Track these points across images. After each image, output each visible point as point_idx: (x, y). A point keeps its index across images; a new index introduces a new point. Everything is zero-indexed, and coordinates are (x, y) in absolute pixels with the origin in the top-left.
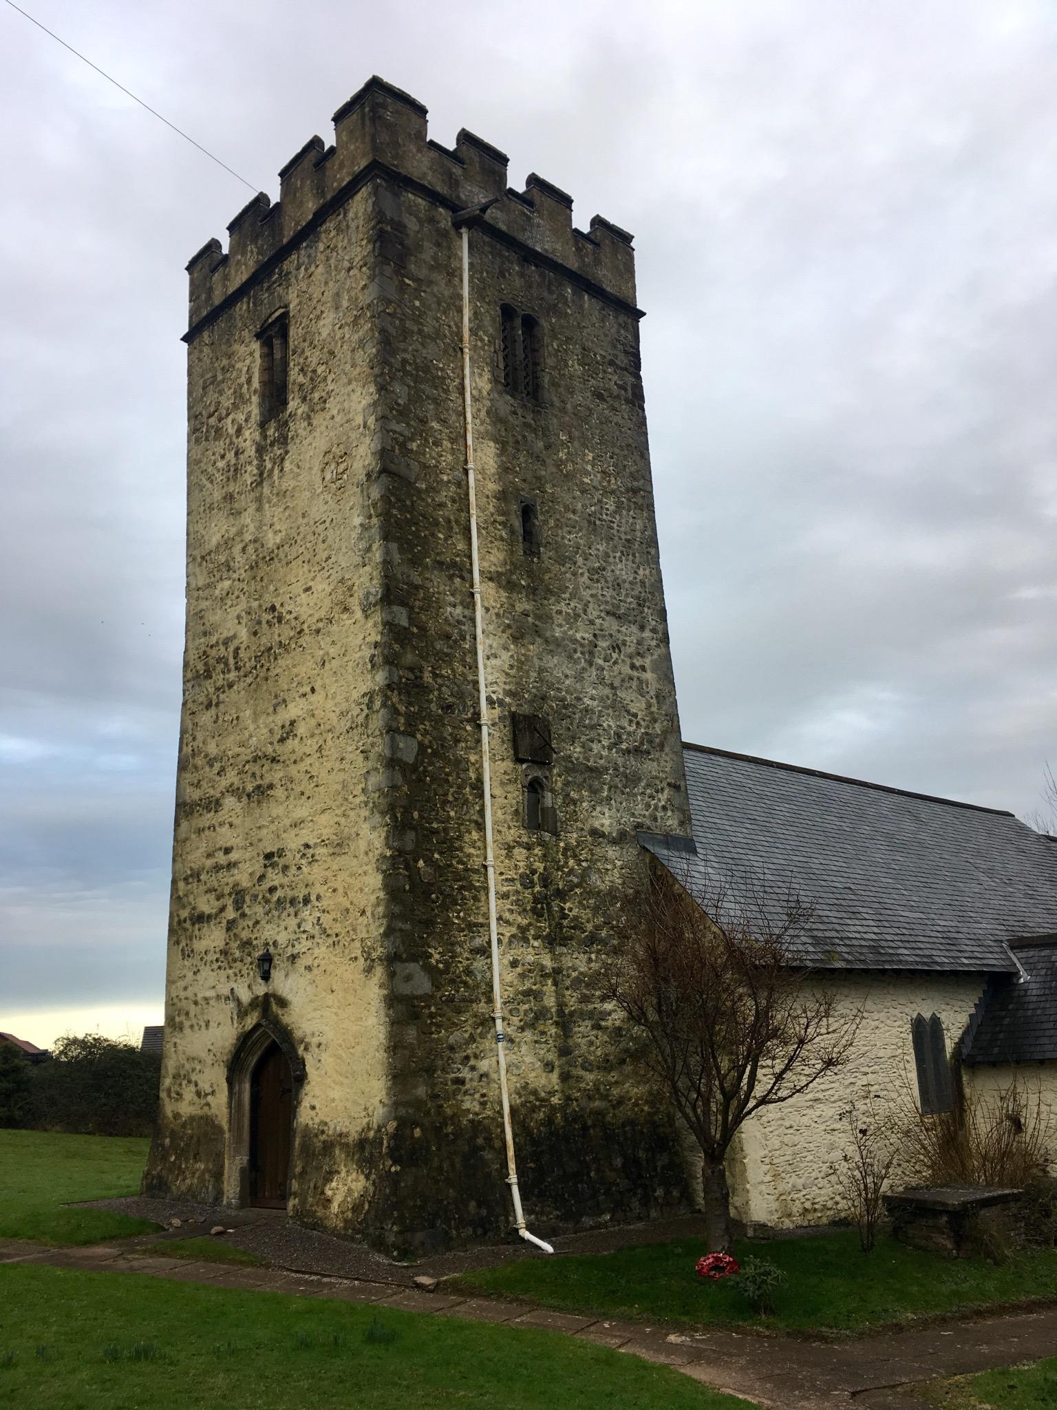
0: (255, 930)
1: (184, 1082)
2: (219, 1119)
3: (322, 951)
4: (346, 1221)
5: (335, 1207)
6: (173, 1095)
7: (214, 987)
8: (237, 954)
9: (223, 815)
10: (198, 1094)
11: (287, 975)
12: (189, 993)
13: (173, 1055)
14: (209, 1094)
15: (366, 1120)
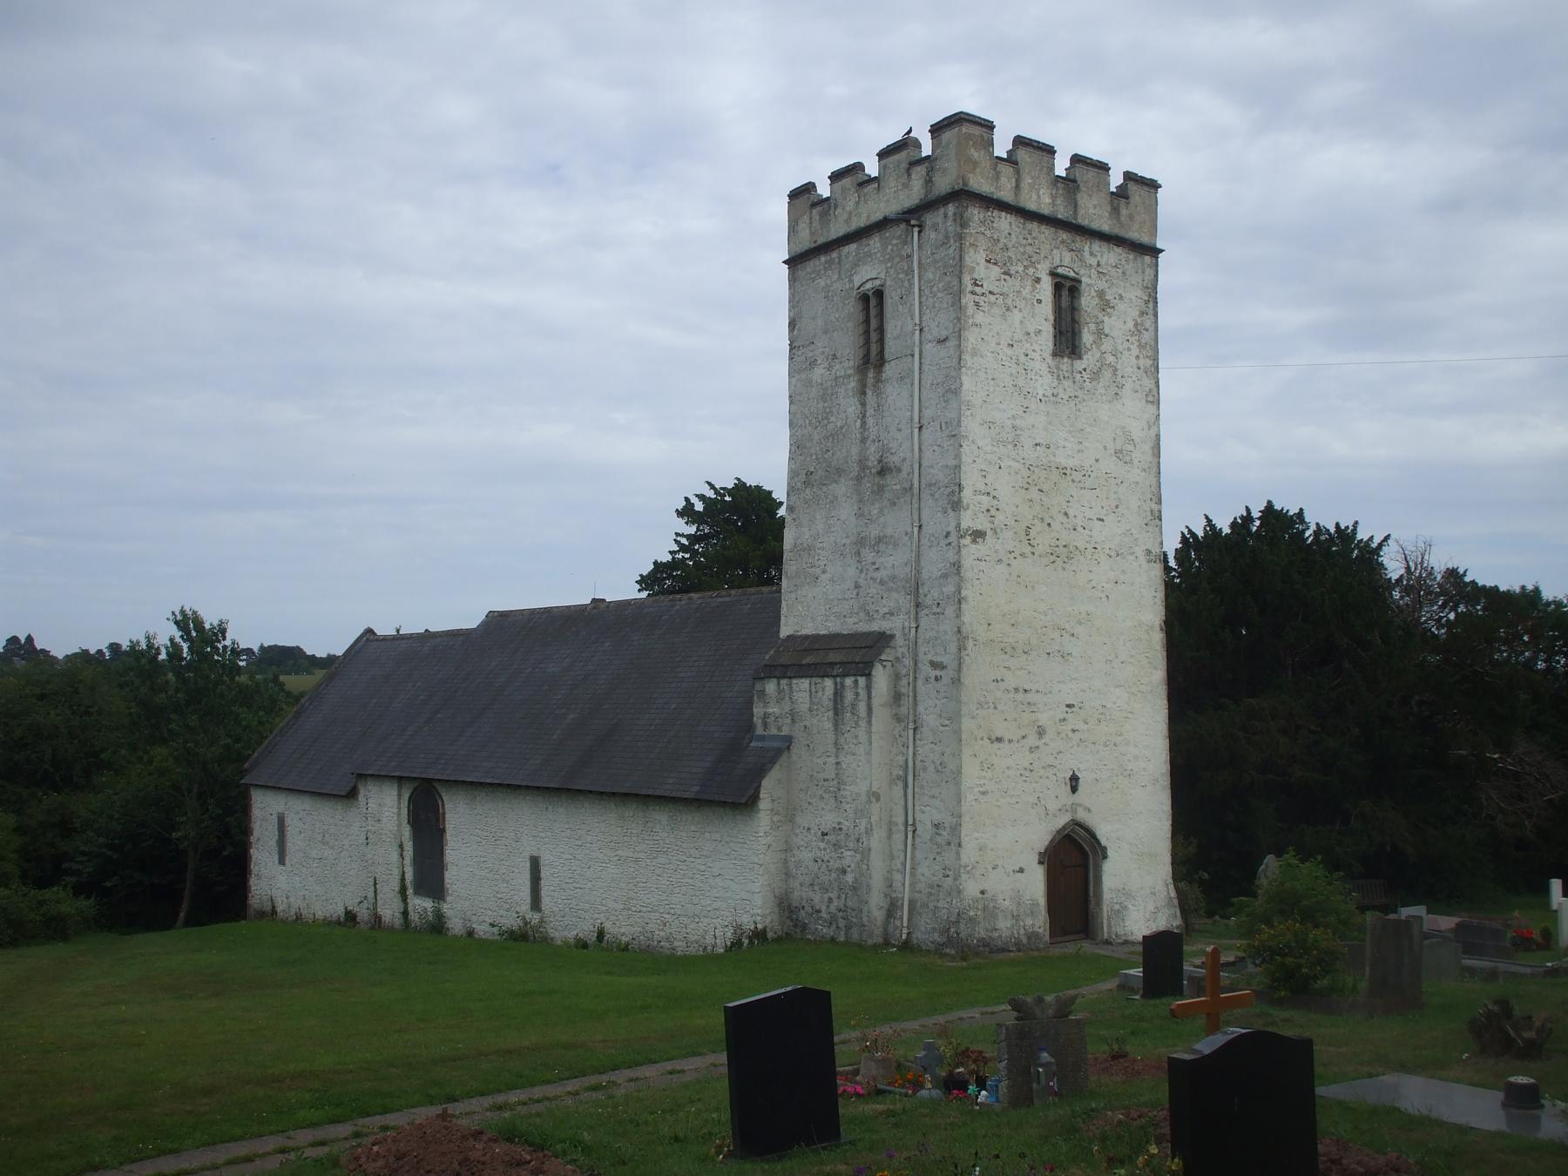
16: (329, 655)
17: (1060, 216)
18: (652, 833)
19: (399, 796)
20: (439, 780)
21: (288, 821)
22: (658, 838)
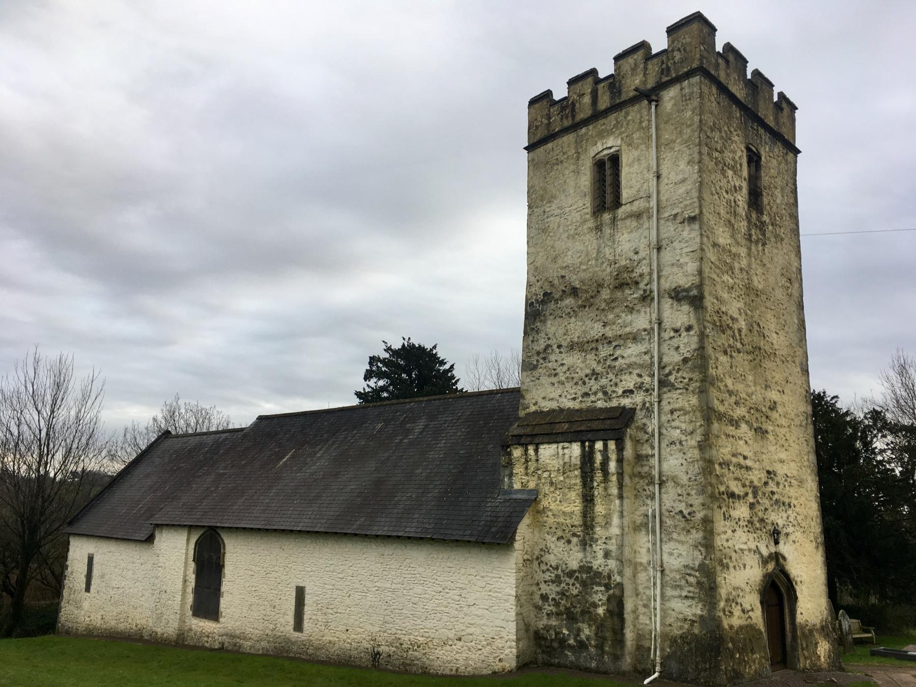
0: (766, 514)
1: (733, 605)
2: (758, 625)
3: (798, 534)
4: (828, 664)
5: (822, 659)
6: (727, 613)
7: (746, 543)
8: (758, 525)
9: (738, 433)
10: (743, 611)
11: (785, 543)
12: (730, 544)
13: (724, 586)
14: (750, 611)
15: (821, 617)
17: (759, 114)
18: (410, 569)
19: (188, 540)
20: (223, 528)
21: (96, 560)
22: (415, 572)
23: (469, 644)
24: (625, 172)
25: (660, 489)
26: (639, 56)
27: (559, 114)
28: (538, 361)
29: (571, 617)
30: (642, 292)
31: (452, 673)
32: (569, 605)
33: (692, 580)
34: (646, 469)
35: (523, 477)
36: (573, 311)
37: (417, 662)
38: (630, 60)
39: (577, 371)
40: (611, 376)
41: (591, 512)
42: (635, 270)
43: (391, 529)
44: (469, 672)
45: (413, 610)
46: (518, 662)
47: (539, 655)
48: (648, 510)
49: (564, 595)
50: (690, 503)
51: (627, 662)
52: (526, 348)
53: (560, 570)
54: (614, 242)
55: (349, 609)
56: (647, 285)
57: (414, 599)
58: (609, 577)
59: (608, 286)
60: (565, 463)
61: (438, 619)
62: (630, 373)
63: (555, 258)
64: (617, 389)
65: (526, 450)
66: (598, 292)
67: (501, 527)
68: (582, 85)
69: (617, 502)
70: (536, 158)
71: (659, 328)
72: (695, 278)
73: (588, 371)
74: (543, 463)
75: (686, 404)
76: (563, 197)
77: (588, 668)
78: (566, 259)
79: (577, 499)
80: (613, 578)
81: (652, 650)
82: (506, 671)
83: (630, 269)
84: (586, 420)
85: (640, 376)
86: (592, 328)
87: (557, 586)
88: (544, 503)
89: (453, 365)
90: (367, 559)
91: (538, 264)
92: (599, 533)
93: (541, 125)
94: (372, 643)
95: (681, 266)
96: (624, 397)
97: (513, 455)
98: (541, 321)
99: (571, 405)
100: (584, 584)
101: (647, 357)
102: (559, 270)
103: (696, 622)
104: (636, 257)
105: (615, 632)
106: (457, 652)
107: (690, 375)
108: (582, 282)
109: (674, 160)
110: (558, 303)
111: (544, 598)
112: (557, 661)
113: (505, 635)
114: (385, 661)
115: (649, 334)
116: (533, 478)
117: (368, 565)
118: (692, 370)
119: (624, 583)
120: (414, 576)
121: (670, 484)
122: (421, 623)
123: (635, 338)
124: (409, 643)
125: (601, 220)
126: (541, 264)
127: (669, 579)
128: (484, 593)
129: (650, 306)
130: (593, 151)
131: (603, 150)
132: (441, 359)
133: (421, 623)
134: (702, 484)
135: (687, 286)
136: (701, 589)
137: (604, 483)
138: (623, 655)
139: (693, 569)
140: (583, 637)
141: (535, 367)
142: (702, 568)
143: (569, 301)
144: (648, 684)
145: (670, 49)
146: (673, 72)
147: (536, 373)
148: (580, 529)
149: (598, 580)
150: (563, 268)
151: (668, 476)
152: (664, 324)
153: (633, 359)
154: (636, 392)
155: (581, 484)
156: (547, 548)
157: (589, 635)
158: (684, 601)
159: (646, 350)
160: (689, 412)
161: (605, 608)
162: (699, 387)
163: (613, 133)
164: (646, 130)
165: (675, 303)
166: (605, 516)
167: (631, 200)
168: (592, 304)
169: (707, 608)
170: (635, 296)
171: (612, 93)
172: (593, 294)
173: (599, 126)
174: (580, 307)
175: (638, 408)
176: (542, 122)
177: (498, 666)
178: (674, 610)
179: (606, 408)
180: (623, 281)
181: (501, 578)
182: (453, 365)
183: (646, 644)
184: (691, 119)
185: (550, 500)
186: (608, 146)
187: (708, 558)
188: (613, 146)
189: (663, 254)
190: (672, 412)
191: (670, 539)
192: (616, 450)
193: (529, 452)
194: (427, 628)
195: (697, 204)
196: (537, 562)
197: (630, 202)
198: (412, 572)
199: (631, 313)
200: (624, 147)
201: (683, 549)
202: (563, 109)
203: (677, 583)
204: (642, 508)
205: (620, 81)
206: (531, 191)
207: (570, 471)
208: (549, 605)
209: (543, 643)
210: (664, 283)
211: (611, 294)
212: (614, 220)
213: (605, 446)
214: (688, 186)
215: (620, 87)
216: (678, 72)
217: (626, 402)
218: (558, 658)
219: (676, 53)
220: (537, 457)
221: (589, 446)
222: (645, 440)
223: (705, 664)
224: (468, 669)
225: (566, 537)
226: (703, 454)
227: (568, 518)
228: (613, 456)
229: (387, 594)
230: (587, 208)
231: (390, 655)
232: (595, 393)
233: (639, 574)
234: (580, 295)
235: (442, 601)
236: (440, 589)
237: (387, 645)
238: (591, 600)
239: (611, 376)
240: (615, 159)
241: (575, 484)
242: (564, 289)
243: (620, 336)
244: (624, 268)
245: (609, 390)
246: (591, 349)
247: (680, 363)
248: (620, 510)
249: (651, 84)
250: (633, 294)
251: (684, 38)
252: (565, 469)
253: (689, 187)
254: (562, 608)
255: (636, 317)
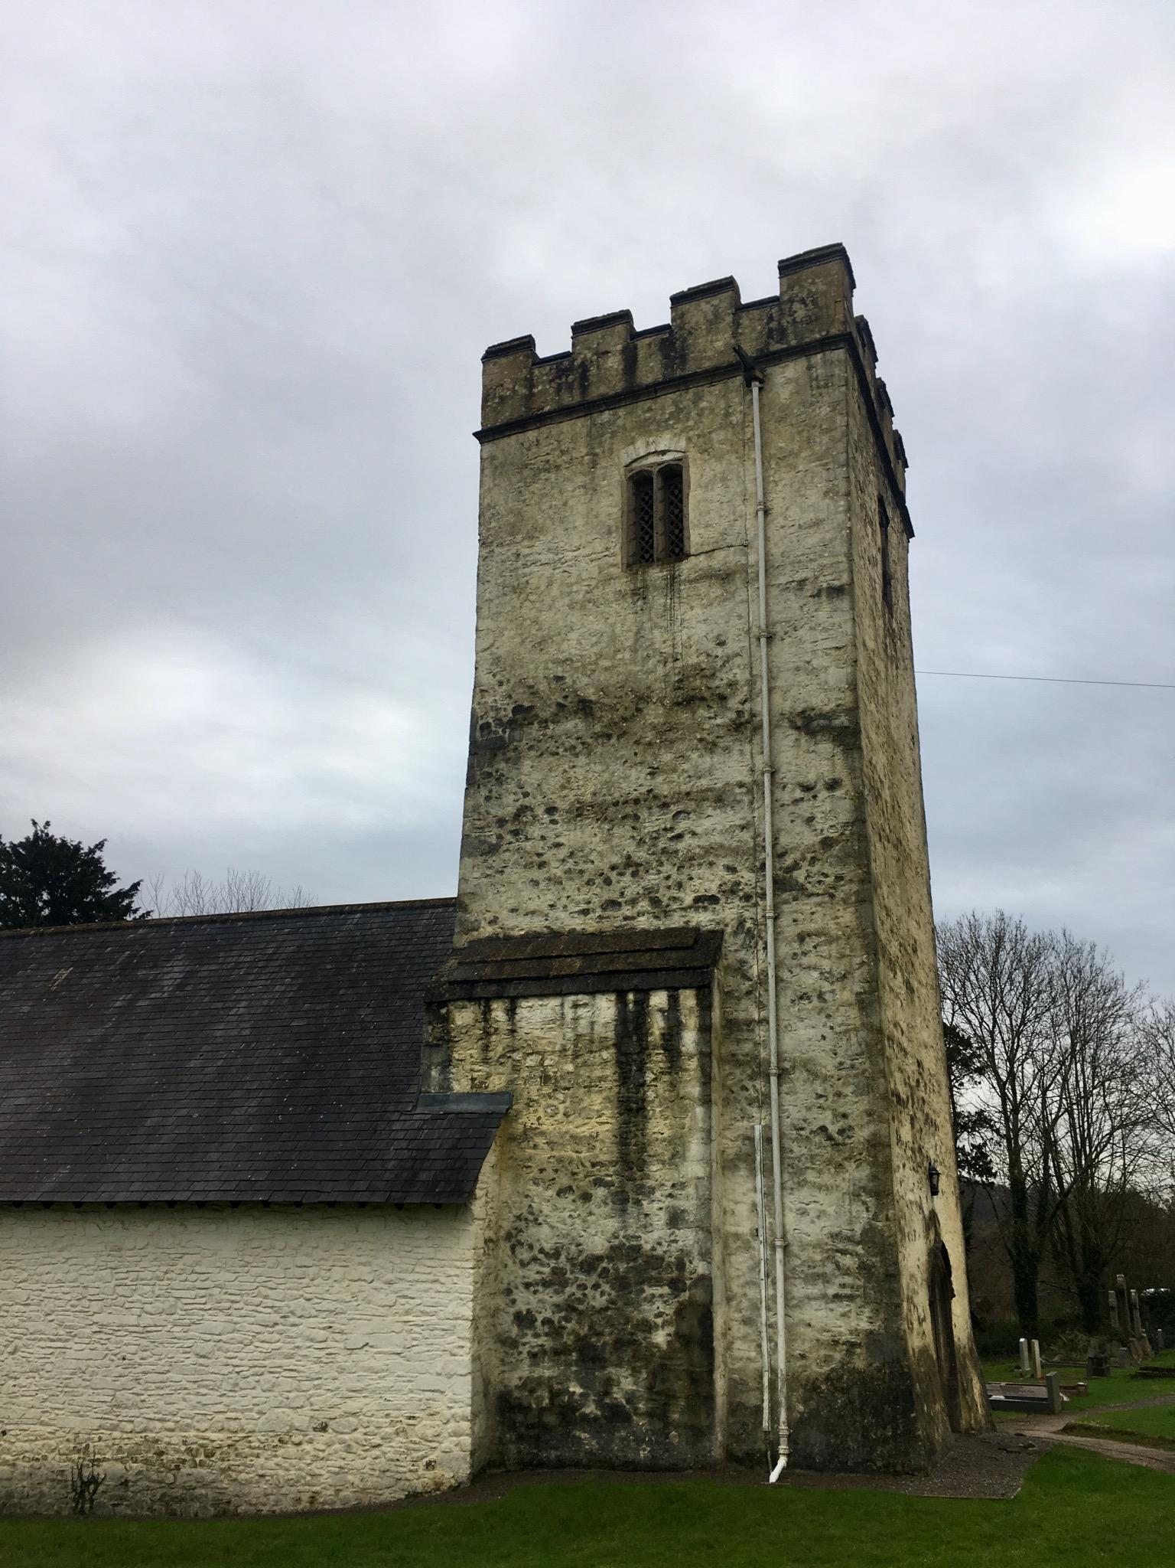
16: (689, 289)
18: (194, 1276)
22: (207, 1284)
23: (346, 1437)
24: (696, 501)
25: (779, 1085)
26: (722, 300)
27: (553, 380)
28: (500, 837)
29: (589, 1356)
30: (734, 716)
31: (300, 1507)
32: (584, 1331)
33: (847, 1261)
34: (747, 1047)
35: (477, 1067)
36: (583, 743)
37: (203, 1491)
38: (705, 306)
39: (592, 858)
40: (667, 868)
41: (639, 1133)
42: (718, 674)
43: (153, 1186)
44: (345, 1501)
45: (196, 1372)
46: (472, 1466)
47: (512, 1447)
48: (753, 1128)
49: (574, 1309)
50: (841, 1110)
51: (717, 1442)
52: (471, 812)
53: (563, 1258)
54: (672, 621)
55: (11, 1382)
56: (744, 702)
57: (201, 1344)
58: (681, 1265)
59: (661, 700)
60: (578, 1036)
61: (266, 1387)
62: (711, 864)
63: (540, 643)
64: (681, 895)
65: (487, 1011)
66: (639, 710)
67: (443, 1170)
68: (603, 337)
69: (699, 1111)
70: (499, 454)
71: (773, 783)
72: (842, 695)
73: (616, 859)
74: (525, 1037)
75: (832, 925)
76: (560, 531)
77: (632, 1462)
78: (565, 646)
79: (606, 1108)
80: (689, 1267)
81: (766, 1412)
82: (444, 1488)
83: (708, 673)
84: (619, 952)
85: (731, 869)
86: (626, 778)
87: (557, 1292)
88: (528, 1119)
89: (138, 884)
90: (71, 1262)
91: (501, 652)
92: (657, 1175)
93: (511, 397)
94: (75, 1456)
95: (814, 672)
96: (697, 909)
97: (453, 1022)
98: (507, 761)
99: (577, 923)
100: (622, 1284)
101: (746, 836)
102: (550, 665)
103: (859, 1346)
104: (719, 651)
105: (694, 1379)
106: (316, 1459)
107: (838, 871)
108: (603, 690)
109: (796, 486)
110: (547, 727)
111: (525, 1320)
112: (553, 1454)
113: (444, 1407)
114: (111, 1498)
115: (750, 791)
116: (501, 1069)
117: (73, 1275)
118: (842, 860)
119: (713, 1276)
120: (203, 1292)
121: (800, 1075)
122: (219, 1399)
123: (720, 799)
124: (183, 1448)
125: (644, 580)
126: (509, 652)
127: (799, 1262)
128: (391, 1318)
129: (750, 741)
130: (626, 455)
131: (649, 454)
132: (105, 872)
133: (219, 1399)
134: (867, 1074)
135: (827, 709)
136: (868, 1280)
137: (670, 1073)
138: (711, 1428)
139: (849, 1239)
140: (618, 1395)
141: (493, 849)
142: (870, 1236)
143: (573, 725)
144: (779, 1479)
145: (786, 298)
146: (792, 336)
147: (496, 861)
148: (612, 1169)
149: (654, 1273)
150: (558, 662)
151: (794, 1060)
152: (782, 776)
153: (717, 839)
154: (723, 900)
155: (616, 1077)
156: (532, 1213)
157: (633, 1392)
158: (832, 1306)
159: (743, 822)
160: (838, 938)
161: (671, 1329)
162: (857, 893)
163: (668, 428)
164: (738, 429)
165: (804, 739)
166: (670, 1141)
167: (707, 549)
168: (625, 733)
169: (882, 1316)
170: (719, 721)
171: (666, 357)
172: (628, 714)
173: (640, 412)
174: (597, 736)
175: (729, 930)
176: (514, 391)
177: (423, 1480)
178: (809, 1325)
179: (657, 931)
180: (692, 693)
181: (436, 1281)
182: (138, 884)
183: (751, 1400)
184: (831, 420)
185: (541, 1113)
186: (659, 449)
187: (882, 1217)
188: (669, 451)
189: (777, 646)
190: (801, 938)
191: (801, 1184)
192: (696, 1009)
193: (494, 1014)
194: (235, 1410)
195: (844, 566)
196: (508, 1245)
197: (707, 552)
198: (198, 1284)
199: (712, 752)
200: (693, 454)
201: (827, 1202)
202: (561, 373)
203: (816, 1270)
204: (739, 1124)
205: (685, 340)
206: (488, 514)
207: (591, 1052)
208: (537, 1336)
209: (520, 1418)
210: (781, 701)
211: (667, 715)
212: (672, 581)
213: (674, 1001)
214: (826, 533)
215: (683, 349)
216: (802, 338)
217: (703, 919)
218: (556, 1448)
219: (796, 306)
220: (513, 1024)
221: (636, 1002)
222: (745, 991)
223: (884, 1428)
224: (342, 1494)
225: (578, 1188)
226: (867, 1016)
227: (584, 1149)
228: (691, 1021)
229: (125, 1340)
230: (614, 555)
231: (127, 1481)
232: (633, 902)
233: (733, 1258)
234: (599, 714)
235: (279, 1345)
236: (276, 1318)
237: (122, 1460)
238: (637, 1316)
239: (667, 868)
240: (673, 476)
241: (601, 1079)
242: (560, 700)
243: (688, 794)
244: (695, 669)
245: (664, 895)
246: (624, 818)
247: (817, 847)
248: (705, 1126)
249: (750, 348)
250: (715, 717)
251: (813, 283)
252: (581, 1047)
253: (828, 536)
254: (568, 1339)
255: (721, 760)
